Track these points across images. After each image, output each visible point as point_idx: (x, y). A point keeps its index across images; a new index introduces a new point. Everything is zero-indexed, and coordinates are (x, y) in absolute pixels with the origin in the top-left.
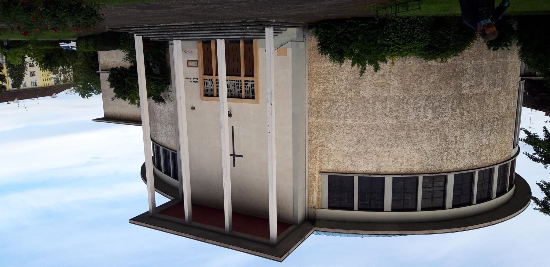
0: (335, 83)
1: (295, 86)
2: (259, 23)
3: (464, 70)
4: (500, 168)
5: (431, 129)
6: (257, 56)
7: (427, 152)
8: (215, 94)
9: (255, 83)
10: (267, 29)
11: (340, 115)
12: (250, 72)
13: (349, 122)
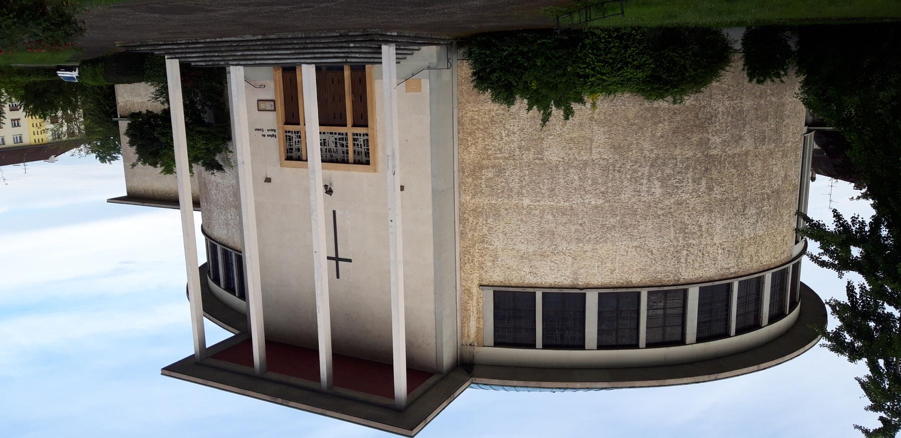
0: (502, 139)
1: (435, 143)
2: (370, 38)
3: (712, 116)
4: (774, 276)
5: (660, 212)
6: (372, 92)
7: (654, 251)
8: (304, 158)
9: (370, 138)
10: (385, 48)
11: (511, 190)
12: (362, 119)
13: (526, 202)
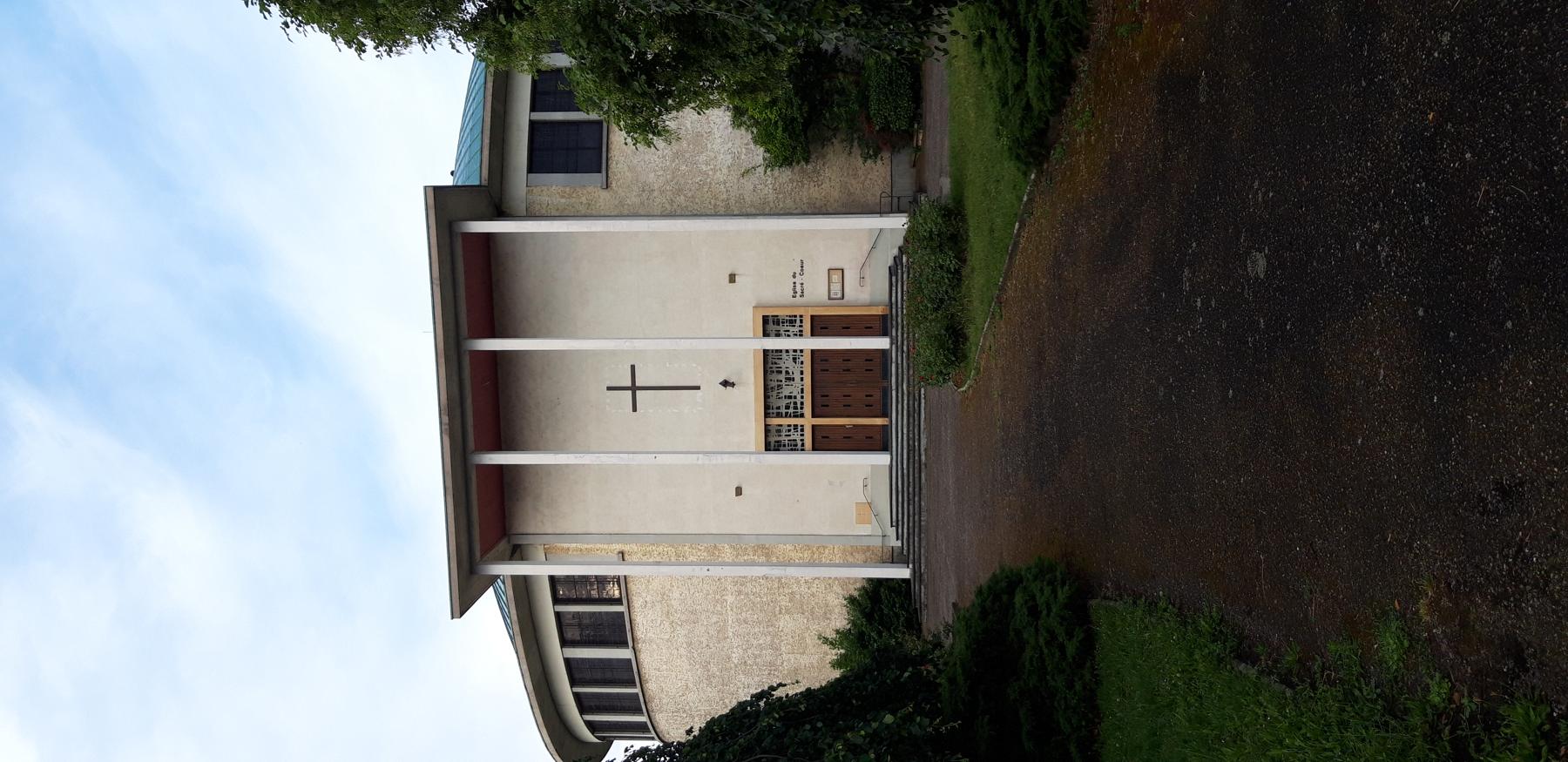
12: (824, 442)
13: (730, 599)
